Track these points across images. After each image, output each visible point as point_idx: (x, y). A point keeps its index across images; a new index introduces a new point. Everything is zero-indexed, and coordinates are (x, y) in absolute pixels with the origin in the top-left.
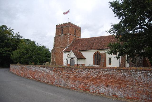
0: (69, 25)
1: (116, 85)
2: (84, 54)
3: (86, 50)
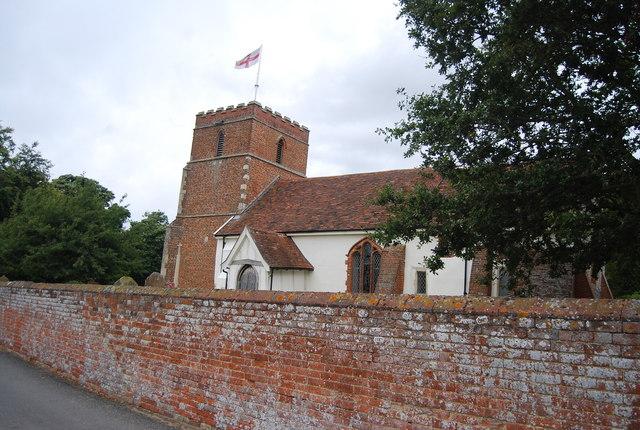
0: (251, 113)
1: (334, 395)
2: (309, 247)
3: (314, 230)
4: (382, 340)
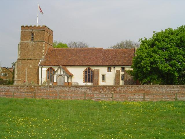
2: (71, 70)
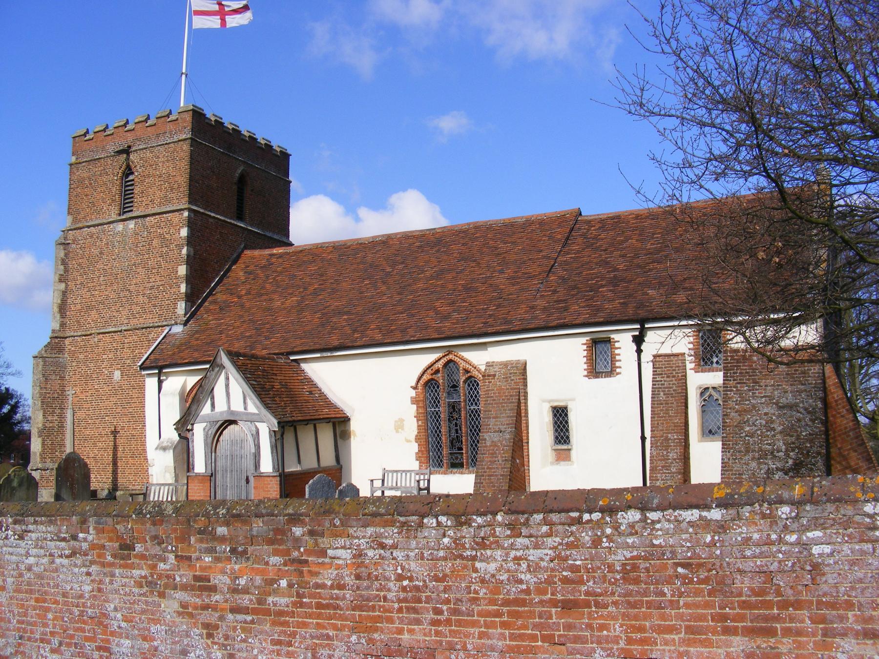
4: (827, 549)
